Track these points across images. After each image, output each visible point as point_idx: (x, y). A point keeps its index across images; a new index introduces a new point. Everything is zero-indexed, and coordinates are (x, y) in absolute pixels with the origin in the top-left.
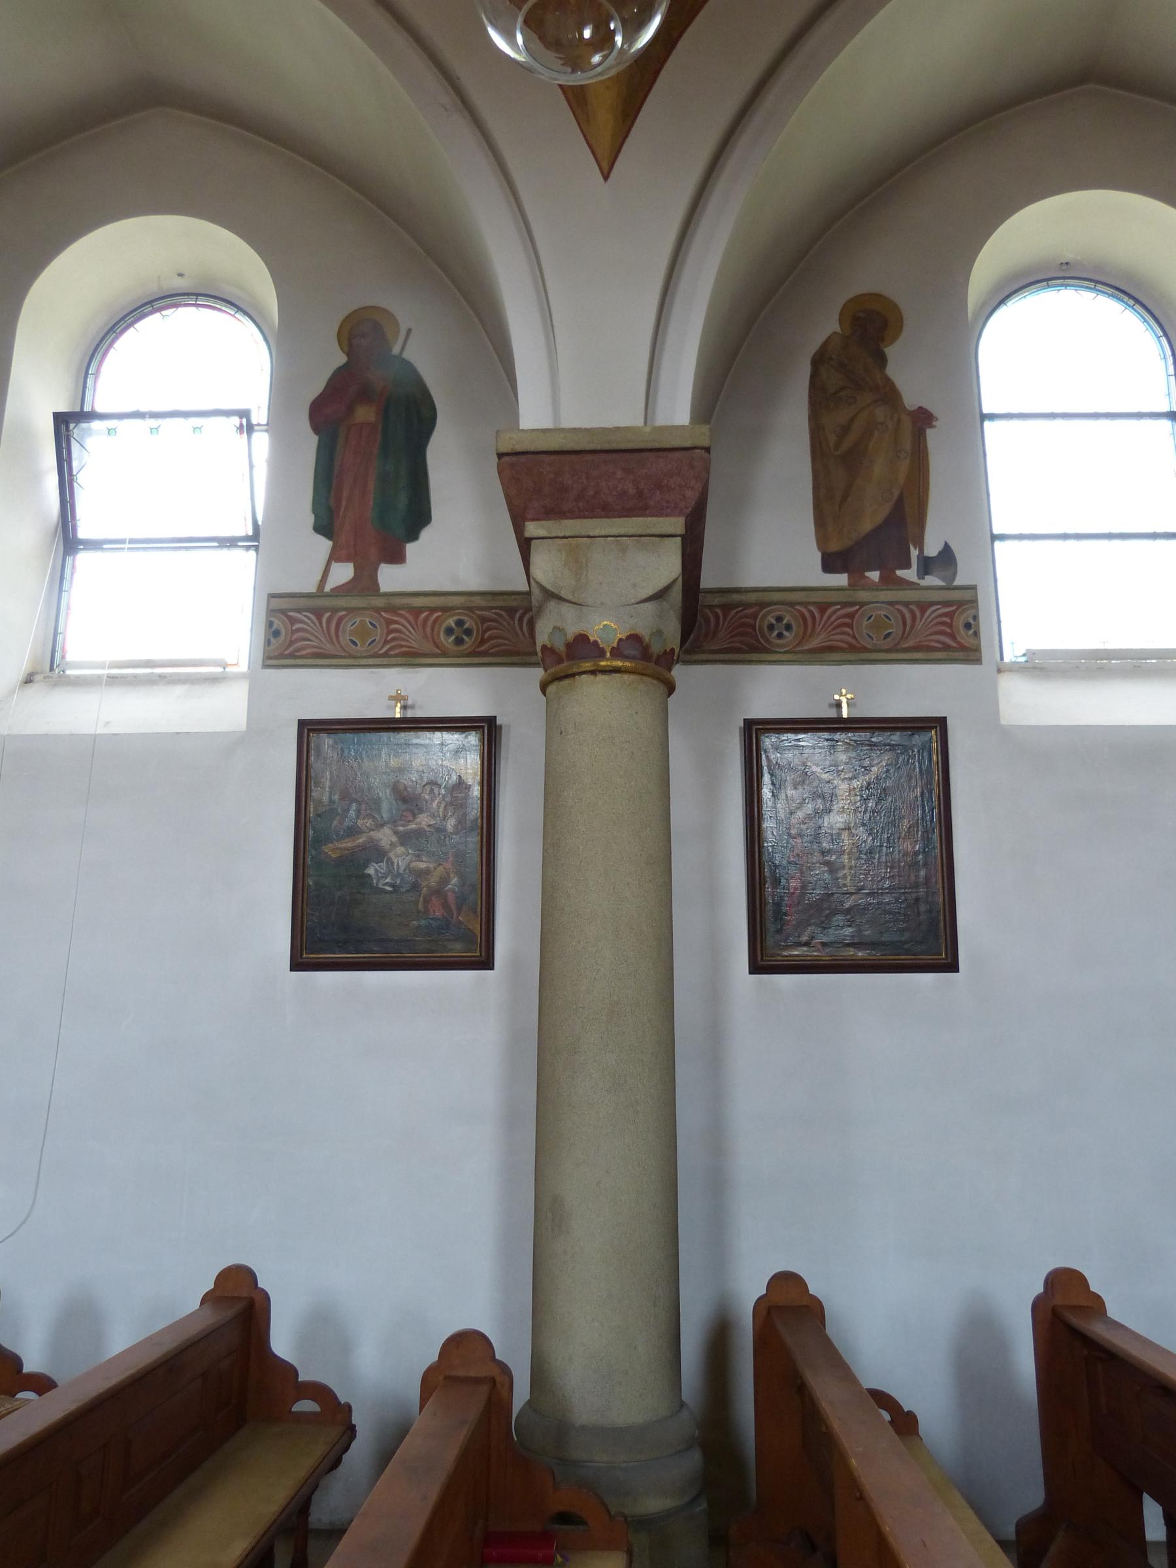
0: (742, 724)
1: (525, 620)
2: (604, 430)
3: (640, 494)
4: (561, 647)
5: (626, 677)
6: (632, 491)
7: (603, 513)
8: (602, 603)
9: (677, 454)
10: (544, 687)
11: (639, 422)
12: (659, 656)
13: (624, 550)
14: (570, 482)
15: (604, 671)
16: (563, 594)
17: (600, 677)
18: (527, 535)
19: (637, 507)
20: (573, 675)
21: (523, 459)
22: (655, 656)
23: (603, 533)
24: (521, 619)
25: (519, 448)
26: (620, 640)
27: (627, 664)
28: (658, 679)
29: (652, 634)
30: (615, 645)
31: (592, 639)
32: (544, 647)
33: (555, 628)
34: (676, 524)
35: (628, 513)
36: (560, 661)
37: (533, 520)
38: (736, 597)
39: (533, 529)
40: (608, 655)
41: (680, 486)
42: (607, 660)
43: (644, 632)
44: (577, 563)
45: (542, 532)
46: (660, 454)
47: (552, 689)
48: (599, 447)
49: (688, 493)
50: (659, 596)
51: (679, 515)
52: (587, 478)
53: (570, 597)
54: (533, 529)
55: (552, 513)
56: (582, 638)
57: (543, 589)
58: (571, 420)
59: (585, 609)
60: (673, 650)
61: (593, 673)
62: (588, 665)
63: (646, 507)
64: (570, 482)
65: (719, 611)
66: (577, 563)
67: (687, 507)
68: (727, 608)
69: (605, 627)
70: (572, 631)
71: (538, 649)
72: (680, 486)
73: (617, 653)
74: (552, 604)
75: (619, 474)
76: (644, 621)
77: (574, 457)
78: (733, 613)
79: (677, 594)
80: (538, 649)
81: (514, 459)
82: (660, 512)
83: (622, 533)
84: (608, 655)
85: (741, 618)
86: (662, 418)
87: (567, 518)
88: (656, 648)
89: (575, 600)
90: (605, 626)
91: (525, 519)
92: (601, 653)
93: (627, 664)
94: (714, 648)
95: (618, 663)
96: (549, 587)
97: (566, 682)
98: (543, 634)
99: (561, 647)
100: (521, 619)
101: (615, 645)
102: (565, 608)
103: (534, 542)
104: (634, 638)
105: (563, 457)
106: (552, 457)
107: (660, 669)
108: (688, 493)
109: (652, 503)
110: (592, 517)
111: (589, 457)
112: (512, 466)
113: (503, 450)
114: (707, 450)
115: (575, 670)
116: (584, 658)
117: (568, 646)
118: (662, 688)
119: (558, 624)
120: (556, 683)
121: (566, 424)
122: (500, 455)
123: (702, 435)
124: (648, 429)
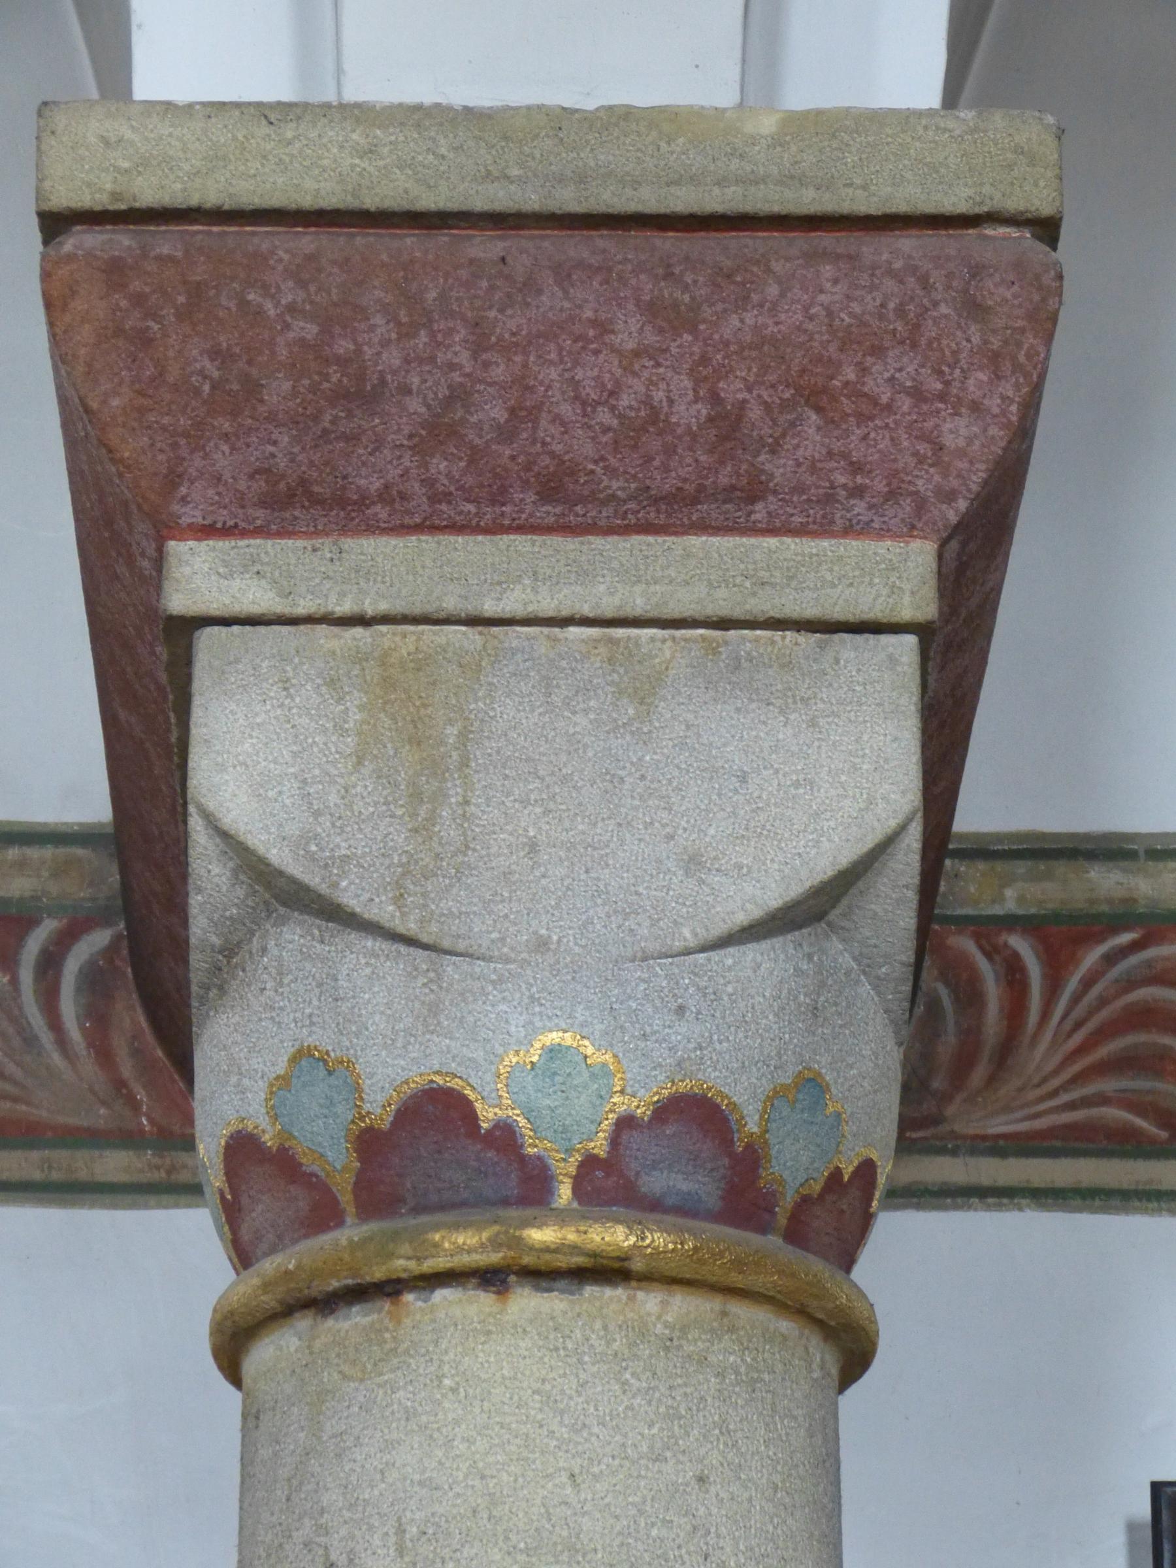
0: (1143, 1508)
1: (72, 967)
2: (559, 120)
3: (727, 426)
4: (330, 1150)
5: (650, 1301)
6: (688, 413)
7: (548, 512)
8: (542, 945)
9: (907, 245)
10: (232, 1345)
11: (714, 87)
12: (805, 1202)
13: (645, 691)
14: (392, 358)
15: (543, 1275)
16: (351, 897)
17: (526, 1302)
18: (179, 601)
19: (708, 482)
20: (391, 1289)
21: (167, 242)
22: (789, 1199)
23: (546, 605)
24: (50, 963)
25: (149, 192)
26: (626, 1123)
27: (658, 1239)
28: (802, 1313)
29: (778, 1094)
30: (600, 1145)
31: (487, 1115)
32: (242, 1149)
33: (302, 1054)
34: (898, 574)
35: (668, 511)
36: (323, 1214)
37: (207, 531)
38: (1107, 882)
39: (200, 576)
40: (564, 1193)
41: (918, 394)
42: (562, 1218)
43: (743, 1092)
44: (420, 746)
45: (254, 596)
46: (826, 240)
47: (267, 1354)
48: (532, 200)
49: (956, 431)
50: (813, 911)
51: (911, 531)
52: (479, 347)
53: (383, 911)
54: (200, 576)
55: (297, 503)
56: (439, 1111)
57: (253, 868)
58: (389, 69)
59: (451, 968)
60: (867, 1169)
61: (492, 1278)
62: (463, 1243)
63: (753, 490)
64: (392, 358)
65: (1020, 944)
66: (420, 746)
67: (949, 497)
68: (1062, 934)
69: (551, 1057)
70: (388, 1074)
71: (209, 1148)
72: (918, 394)
73: (607, 1183)
74: (292, 939)
75: (630, 331)
76: (736, 1034)
77: (410, 241)
78: (1092, 957)
79: (890, 909)
80: (209, 1148)
81: (123, 240)
82: (820, 513)
83: (639, 605)
84: (564, 1193)
85: (1130, 983)
86: (814, 83)
87: (372, 528)
88: (793, 1165)
89: (410, 927)
90: (553, 1052)
91: (166, 529)
92: (533, 1186)
93: (658, 1239)
94: (999, 1126)
95: (614, 1236)
96: (278, 856)
97: (355, 1321)
98: (239, 1075)
99: (330, 1150)
100: (50, 963)
101: (600, 1145)
102: (356, 957)
103: (207, 641)
104: (694, 1113)
105: (363, 240)
106: (307, 241)
107: (817, 1267)
108: (956, 431)
109: (779, 469)
110: (495, 529)
111: (485, 247)
112: (115, 272)
113: (64, 198)
114: (1047, 229)
115: (402, 1265)
116: (455, 1206)
117: (369, 1143)
118: (823, 1357)
119: (323, 1039)
120: (303, 1322)
121: (372, 82)
122: (54, 224)
123: (1003, 161)
124: (767, 125)
